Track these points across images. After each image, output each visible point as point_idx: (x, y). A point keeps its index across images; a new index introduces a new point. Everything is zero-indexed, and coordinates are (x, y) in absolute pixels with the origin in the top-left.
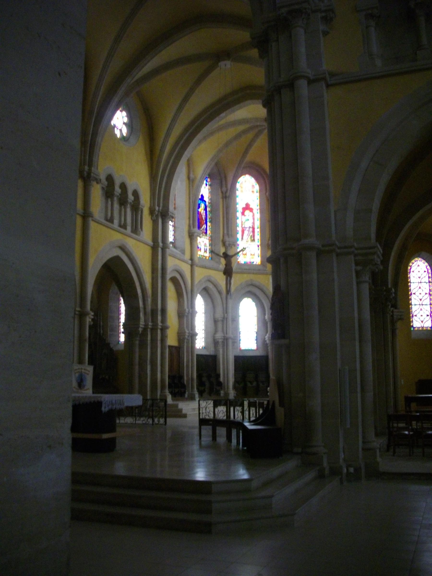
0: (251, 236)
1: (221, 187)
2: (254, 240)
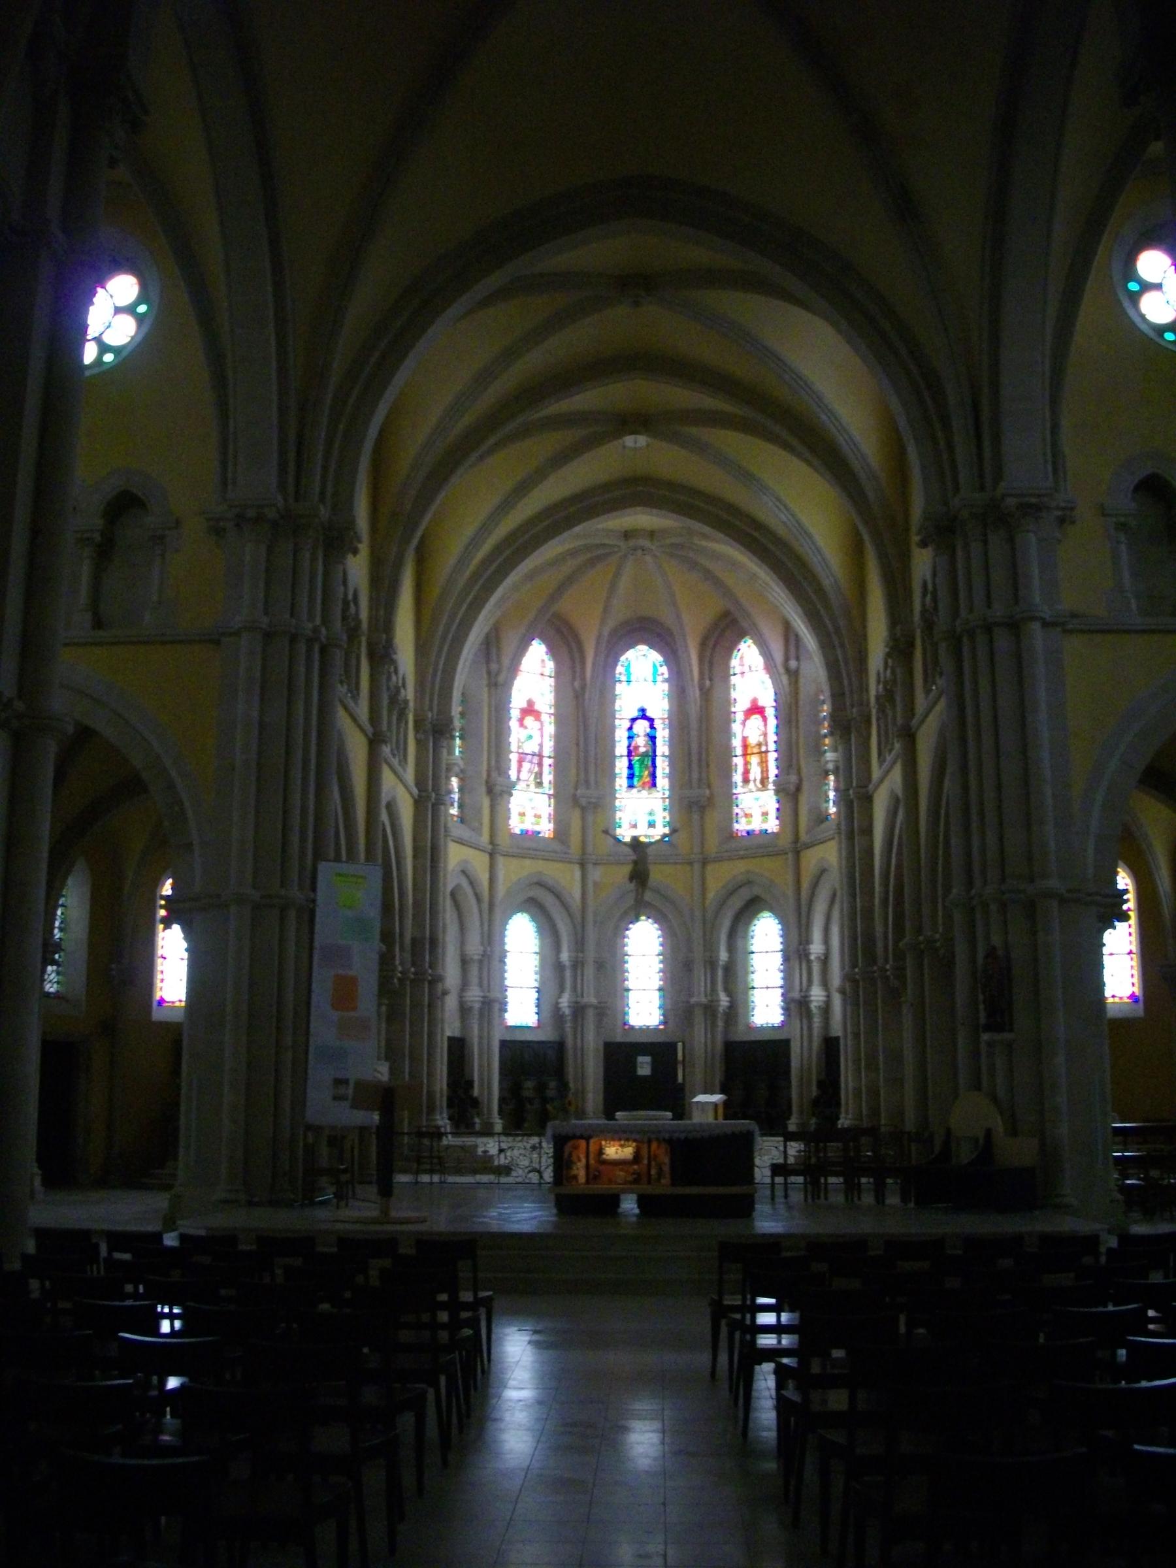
2: (539, 784)
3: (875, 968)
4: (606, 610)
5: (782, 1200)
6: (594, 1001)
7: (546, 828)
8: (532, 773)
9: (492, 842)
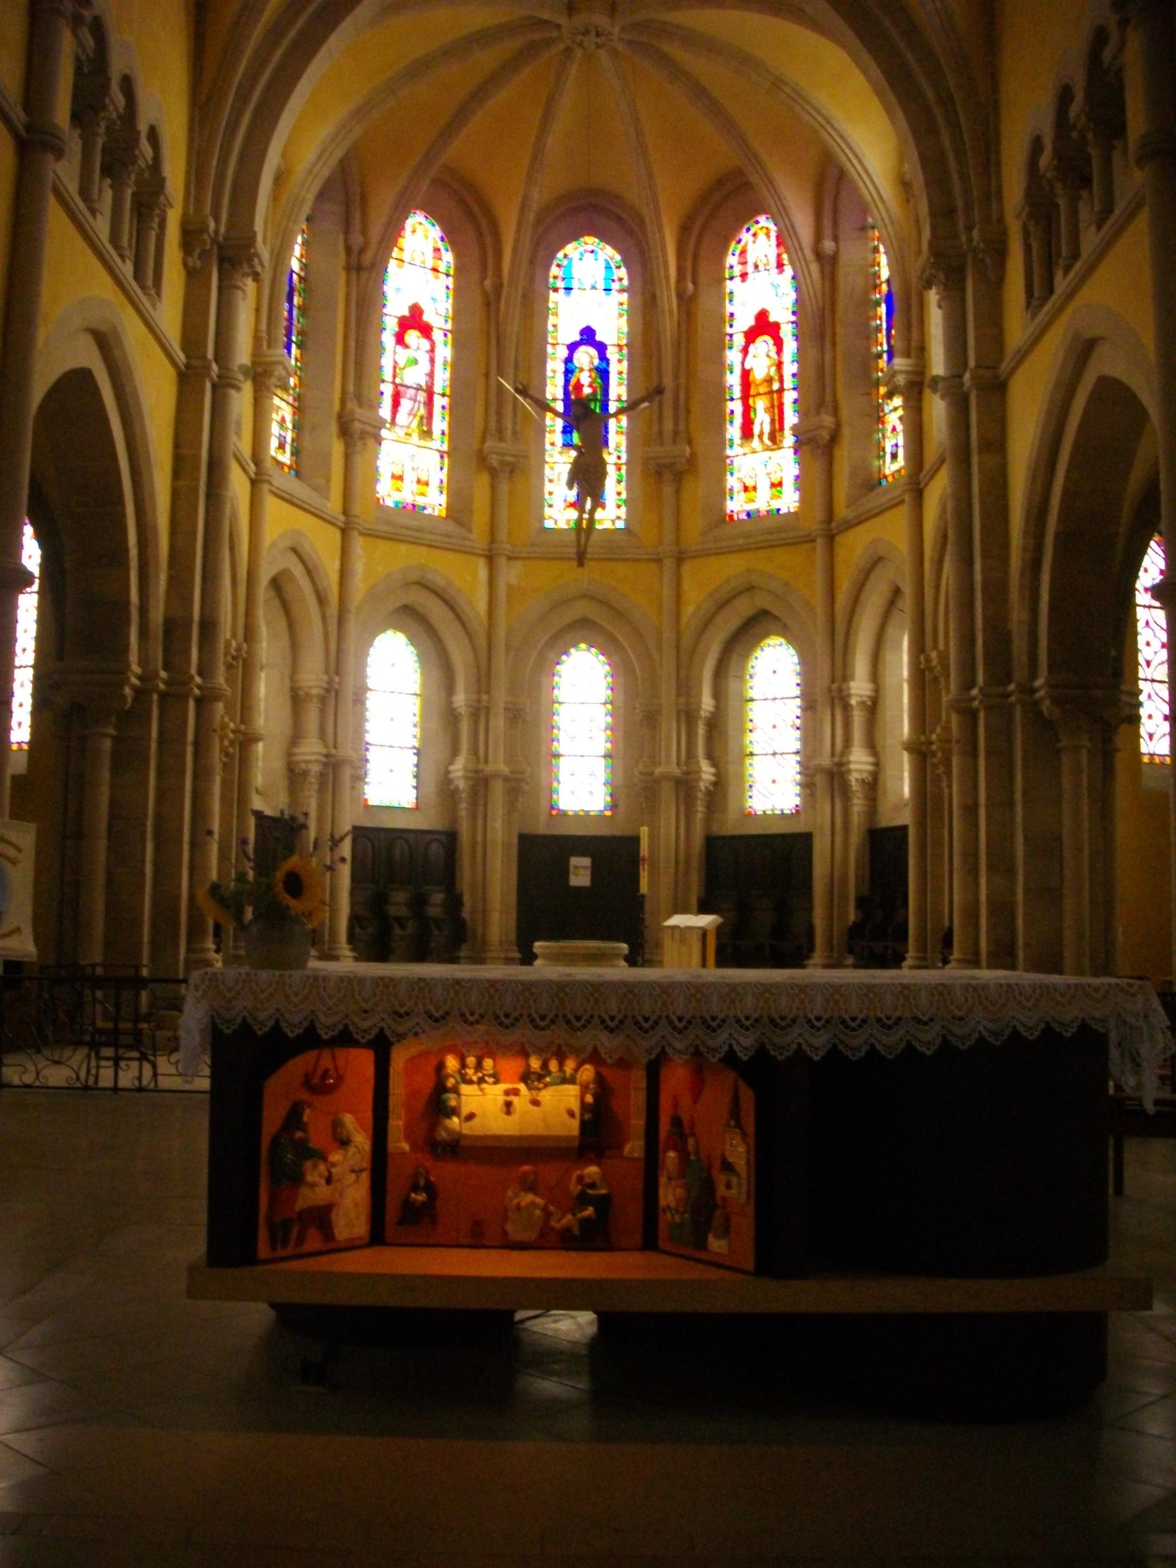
0: (422, 418)
1: (347, 231)
2: (427, 434)
3: (1012, 687)
4: (537, 157)
6: (504, 768)
7: (435, 502)
8: (415, 416)
9: (346, 511)
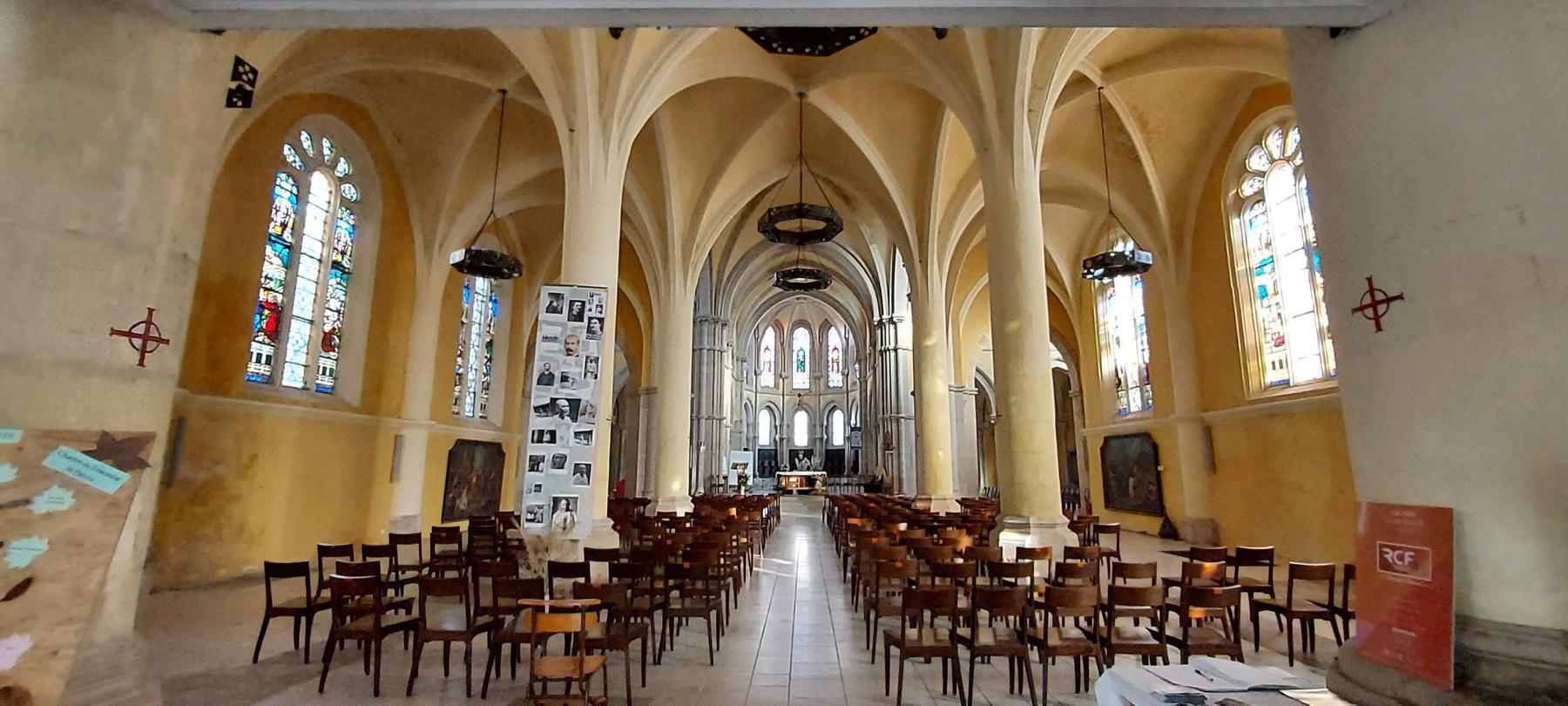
5: (290, 231)
